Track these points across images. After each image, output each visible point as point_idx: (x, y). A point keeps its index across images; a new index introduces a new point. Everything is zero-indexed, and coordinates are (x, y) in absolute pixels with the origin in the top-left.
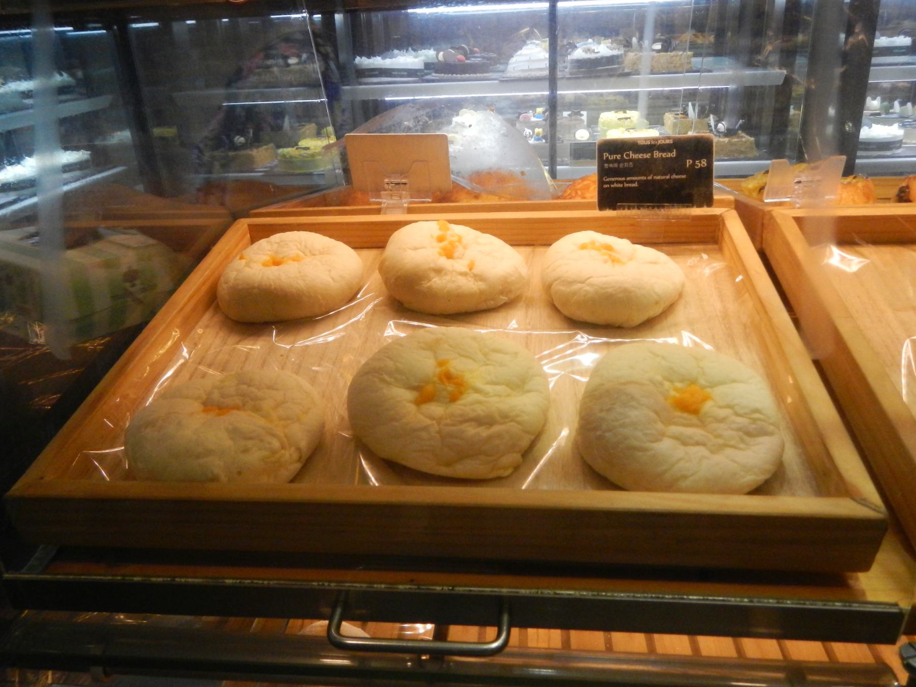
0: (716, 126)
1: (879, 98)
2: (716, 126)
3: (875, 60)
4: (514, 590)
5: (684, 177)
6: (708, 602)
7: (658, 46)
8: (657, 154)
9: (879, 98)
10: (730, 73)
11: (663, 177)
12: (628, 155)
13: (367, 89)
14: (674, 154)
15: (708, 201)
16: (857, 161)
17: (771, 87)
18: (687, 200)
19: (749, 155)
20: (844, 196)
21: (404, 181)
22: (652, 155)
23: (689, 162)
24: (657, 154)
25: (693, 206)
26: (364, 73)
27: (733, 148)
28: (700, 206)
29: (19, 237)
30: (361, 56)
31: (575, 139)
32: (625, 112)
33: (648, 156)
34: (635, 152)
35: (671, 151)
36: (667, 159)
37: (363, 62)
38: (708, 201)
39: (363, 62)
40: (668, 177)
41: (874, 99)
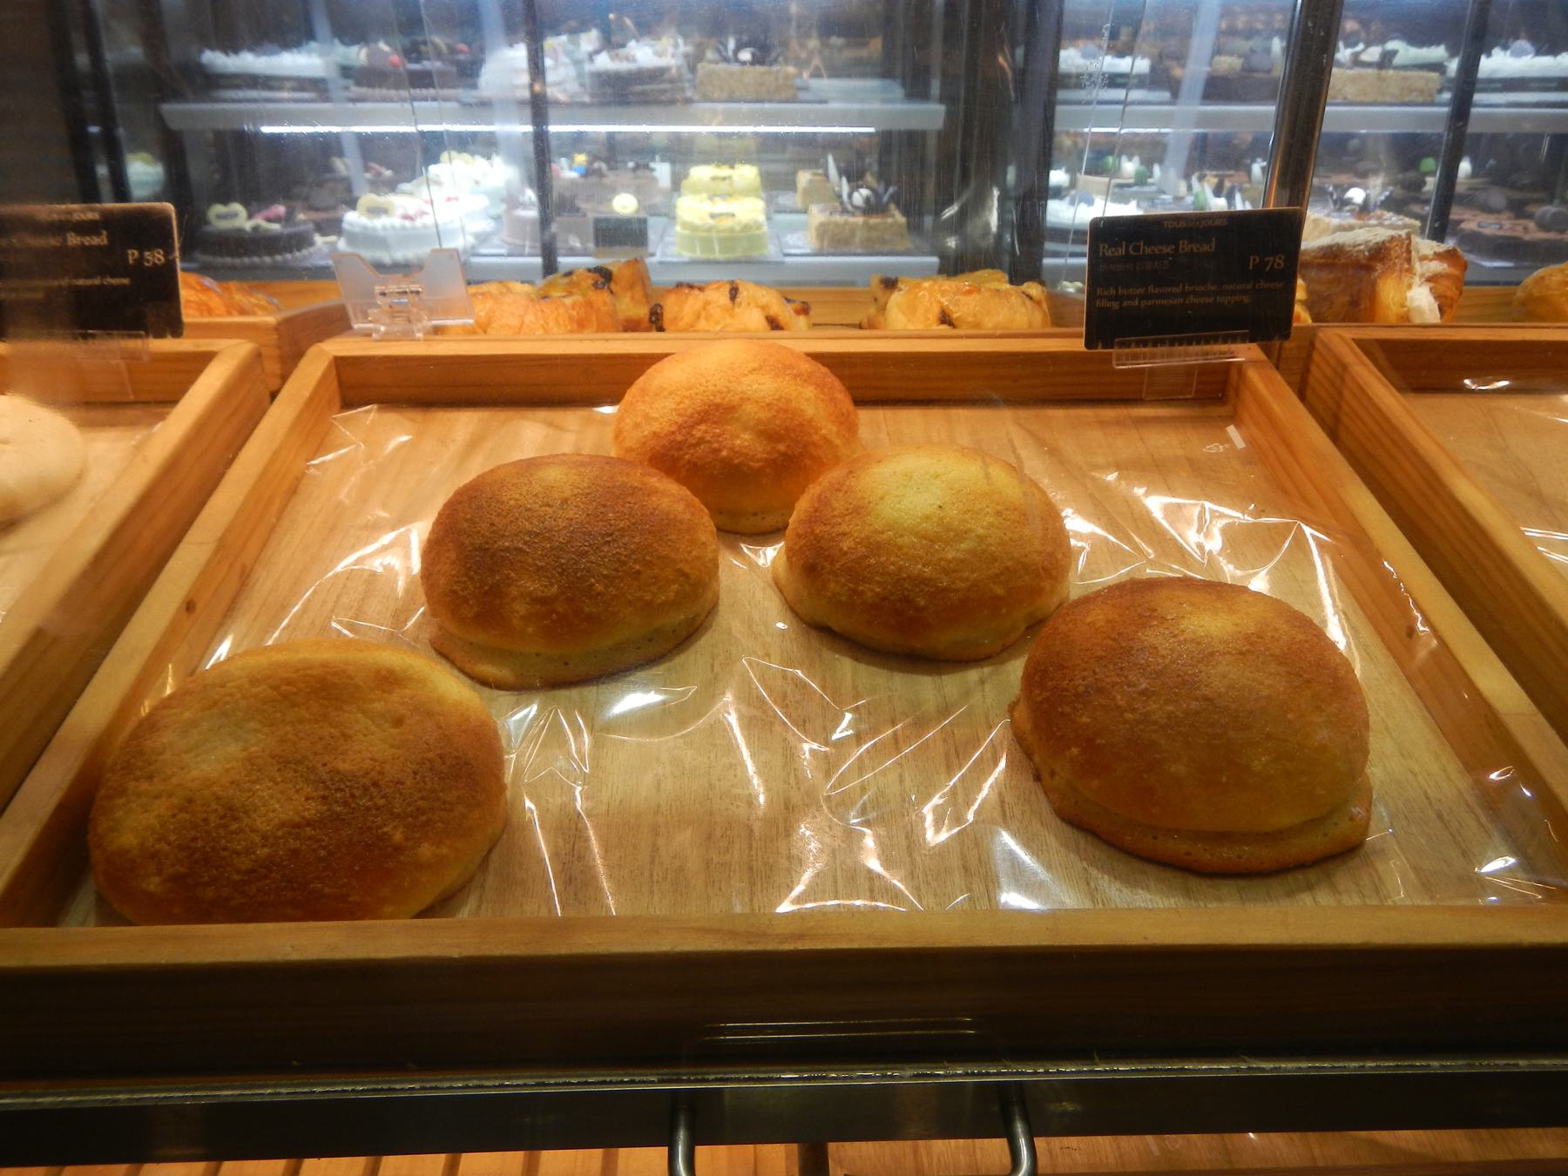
0: (850, 196)
1: (1136, 159)
2: (850, 196)
3: (1062, 94)
4: (31, 1100)
5: (126, 281)
6: (313, 1097)
7: (745, 55)
8: (73, 240)
9: (1136, 159)
10: (876, 106)
11: (89, 282)
12: (1137, 249)
13: (227, 109)
14: (101, 240)
15: (174, 326)
16: (1047, 261)
17: (900, 133)
18: (135, 324)
19: (899, 248)
20: (529, 318)
21: (414, 287)
22: (65, 240)
23: (132, 255)
24: (73, 240)
25: (147, 335)
26: (213, 82)
27: (874, 234)
28: (160, 335)
29: (656, 377)
30: (212, 49)
31: (613, 211)
32: (732, 167)
33: (54, 242)
34: (1149, 243)
35: (99, 234)
36: (91, 247)
37: (217, 60)
38: (174, 326)
39: (217, 60)
40: (97, 282)
41: (1130, 160)
